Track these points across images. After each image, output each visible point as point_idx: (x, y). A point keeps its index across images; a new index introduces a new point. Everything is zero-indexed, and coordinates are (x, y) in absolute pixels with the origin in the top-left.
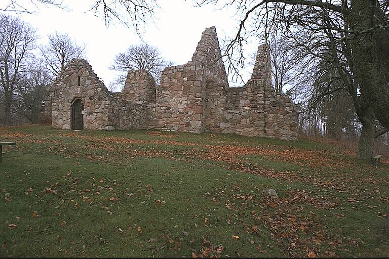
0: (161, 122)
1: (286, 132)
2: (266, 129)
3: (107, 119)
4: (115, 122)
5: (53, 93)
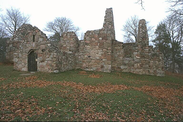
0: (84, 65)
3: (55, 65)
4: (60, 67)
5: (12, 45)
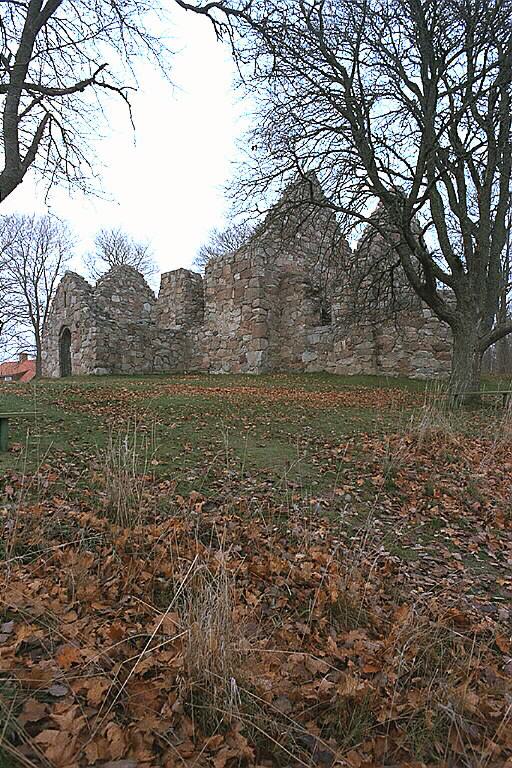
1: (421, 362)
2: (381, 358)
